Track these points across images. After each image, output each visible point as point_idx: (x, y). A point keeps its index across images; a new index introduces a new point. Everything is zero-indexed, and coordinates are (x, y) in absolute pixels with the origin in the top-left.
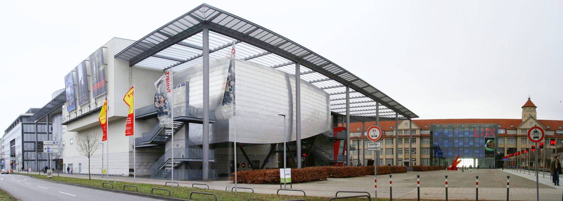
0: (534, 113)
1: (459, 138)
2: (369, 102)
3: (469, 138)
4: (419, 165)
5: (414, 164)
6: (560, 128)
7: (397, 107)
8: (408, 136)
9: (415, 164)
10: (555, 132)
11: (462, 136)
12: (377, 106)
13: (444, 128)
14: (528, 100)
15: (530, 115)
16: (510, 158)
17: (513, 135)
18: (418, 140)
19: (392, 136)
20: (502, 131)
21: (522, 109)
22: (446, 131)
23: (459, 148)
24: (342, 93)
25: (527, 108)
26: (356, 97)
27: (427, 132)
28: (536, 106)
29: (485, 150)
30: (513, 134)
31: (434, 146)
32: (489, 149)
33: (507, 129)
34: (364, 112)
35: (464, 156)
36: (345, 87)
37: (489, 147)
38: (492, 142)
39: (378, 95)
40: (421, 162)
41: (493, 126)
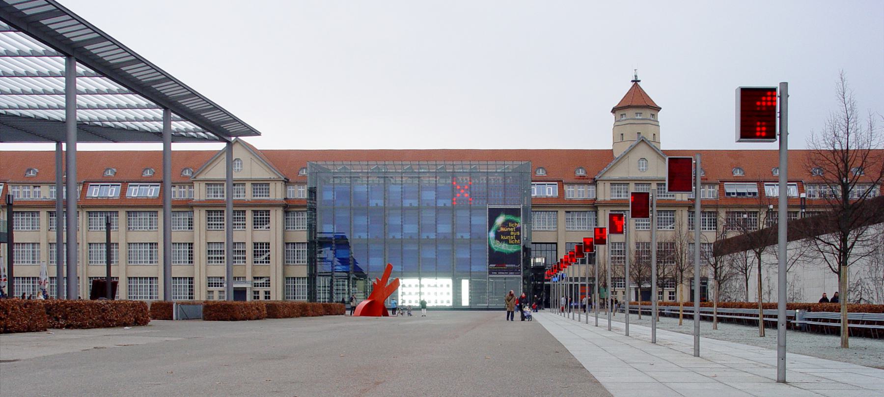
0: (651, 129)
1: (403, 209)
2: (139, 107)
3: (437, 209)
4: (280, 298)
5: (262, 296)
6: (738, 173)
7: (212, 117)
8: (222, 204)
9: (267, 297)
10: (722, 188)
11: (415, 203)
12: (70, 75)
13: (353, 178)
14: (631, 84)
15: (639, 133)
16: (493, 196)
17: (584, 201)
18: (276, 216)
19: (189, 200)
20: (549, 190)
21: (612, 116)
22: (361, 188)
23: (402, 242)
24: (52, 75)
25: (630, 113)
26: (99, 92)
27: (300, 193)
28: (659, 105)
29: (491, 249)
30: (585, 197)
31: (324, 236)
32: (504, 248)
33: (566, 183)
34: (34, 100)
35: (420, 270)
36: (63, 60)
37: (501, 241)
38: (513, 222)
39: (167, 90)
40: (286, 289)
41: (514, 171)
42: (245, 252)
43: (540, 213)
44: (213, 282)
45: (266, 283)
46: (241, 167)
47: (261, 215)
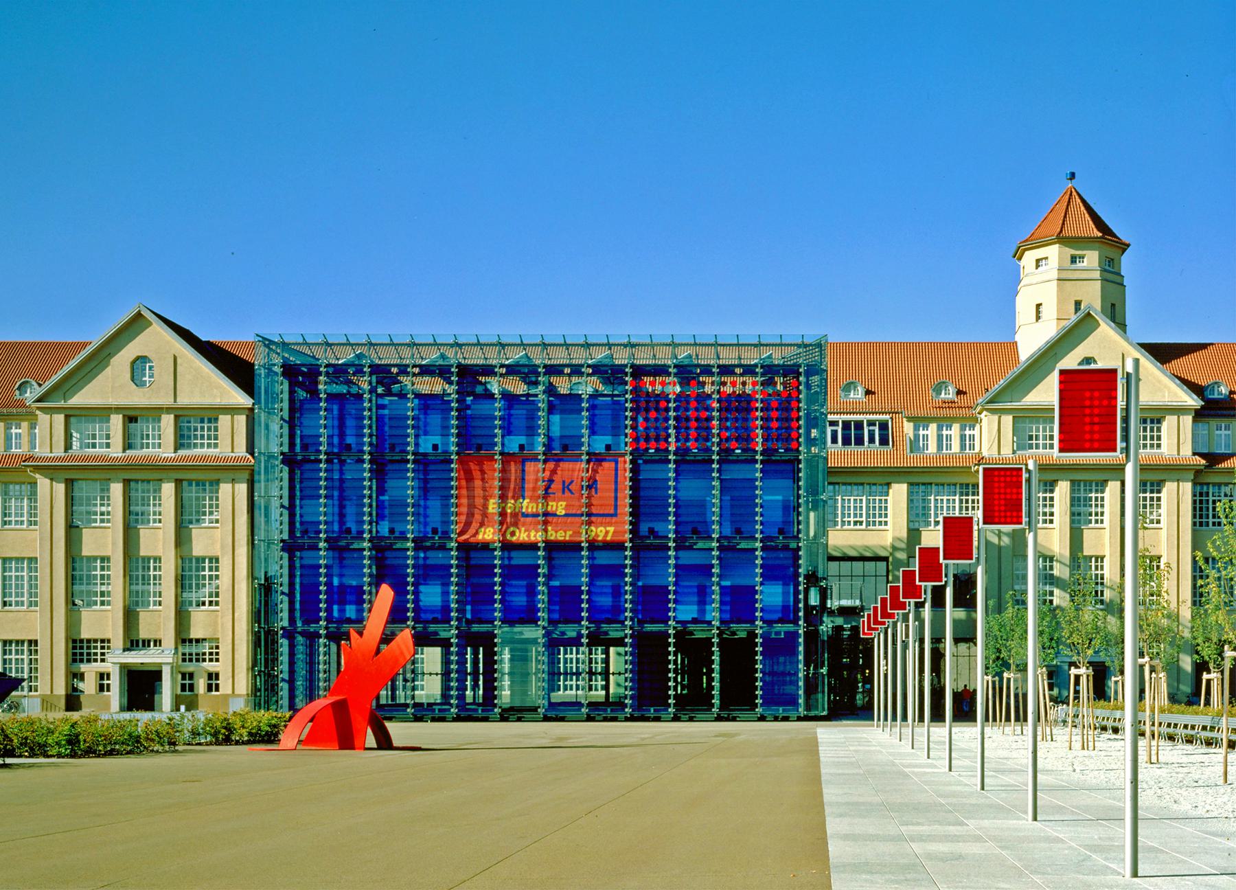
42: (160, 579)
43: (849, 487)
44: (207, 651)
45: (211, 654)
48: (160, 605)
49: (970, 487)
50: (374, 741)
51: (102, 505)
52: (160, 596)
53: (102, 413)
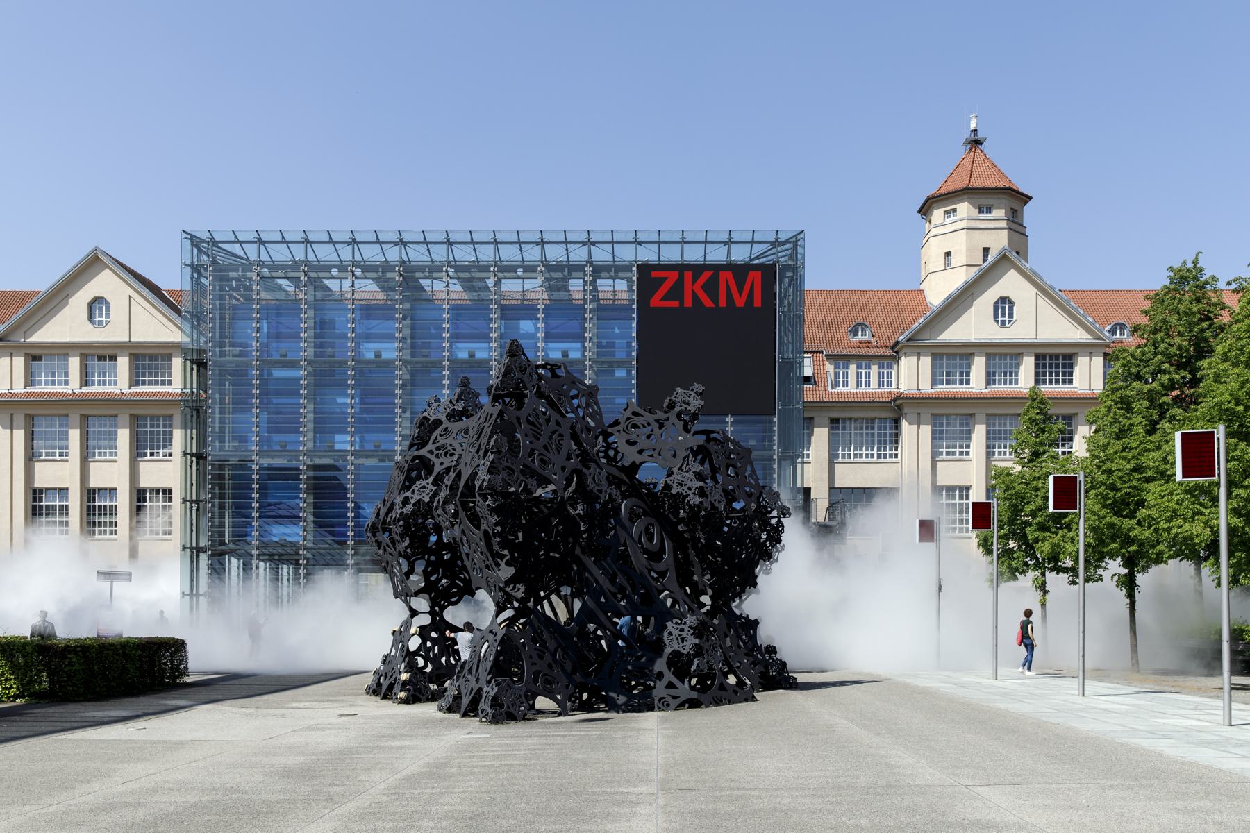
42: (67, 510)
46: (108, 316)
47: (152, 426)
48: (116, 534)
49: (161, 493)
50: (760, 302)
51: (99, 439)
52: (116, 526)
53: (63, 350)
